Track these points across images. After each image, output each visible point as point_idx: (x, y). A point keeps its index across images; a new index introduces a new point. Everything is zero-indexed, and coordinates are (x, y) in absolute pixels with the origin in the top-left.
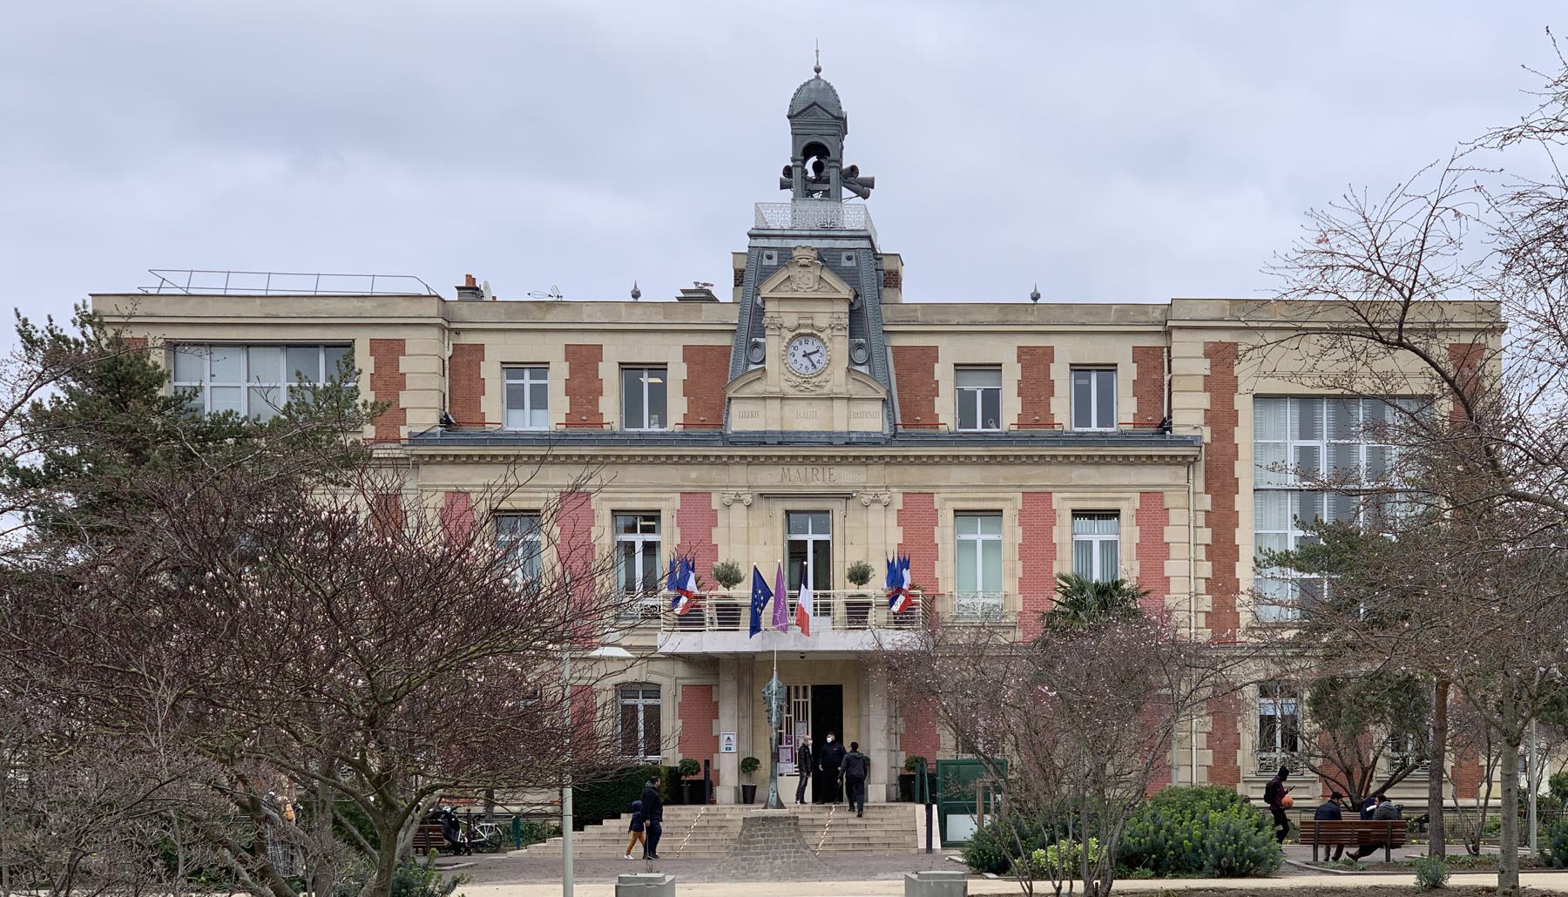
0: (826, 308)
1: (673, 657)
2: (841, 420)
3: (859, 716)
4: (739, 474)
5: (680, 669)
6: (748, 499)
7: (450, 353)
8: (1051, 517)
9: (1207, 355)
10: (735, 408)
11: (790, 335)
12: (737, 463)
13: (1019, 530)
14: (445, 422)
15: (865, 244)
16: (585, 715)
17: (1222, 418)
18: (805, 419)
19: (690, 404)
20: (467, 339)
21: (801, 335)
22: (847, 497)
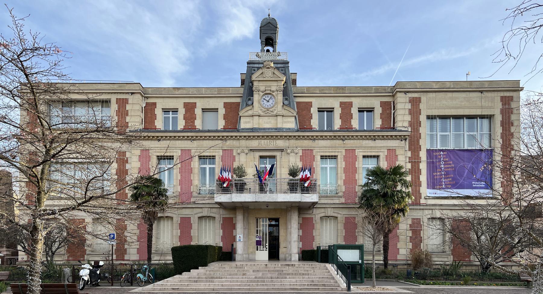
0: (275, 84)
1: (221, 205)
3: (286, 229)
4: (243, 143)
5: (222, 211)
6: (246, 151)
7: (145, 105)
8: (355, 158)
9: (410, 102)
10: (243, 120)
11: (262, 94)
12: (243, 139)
16: (310, 214)
17: (415, 124)
18: (267, 123)
20: (151, 101)
22: (282, 150)
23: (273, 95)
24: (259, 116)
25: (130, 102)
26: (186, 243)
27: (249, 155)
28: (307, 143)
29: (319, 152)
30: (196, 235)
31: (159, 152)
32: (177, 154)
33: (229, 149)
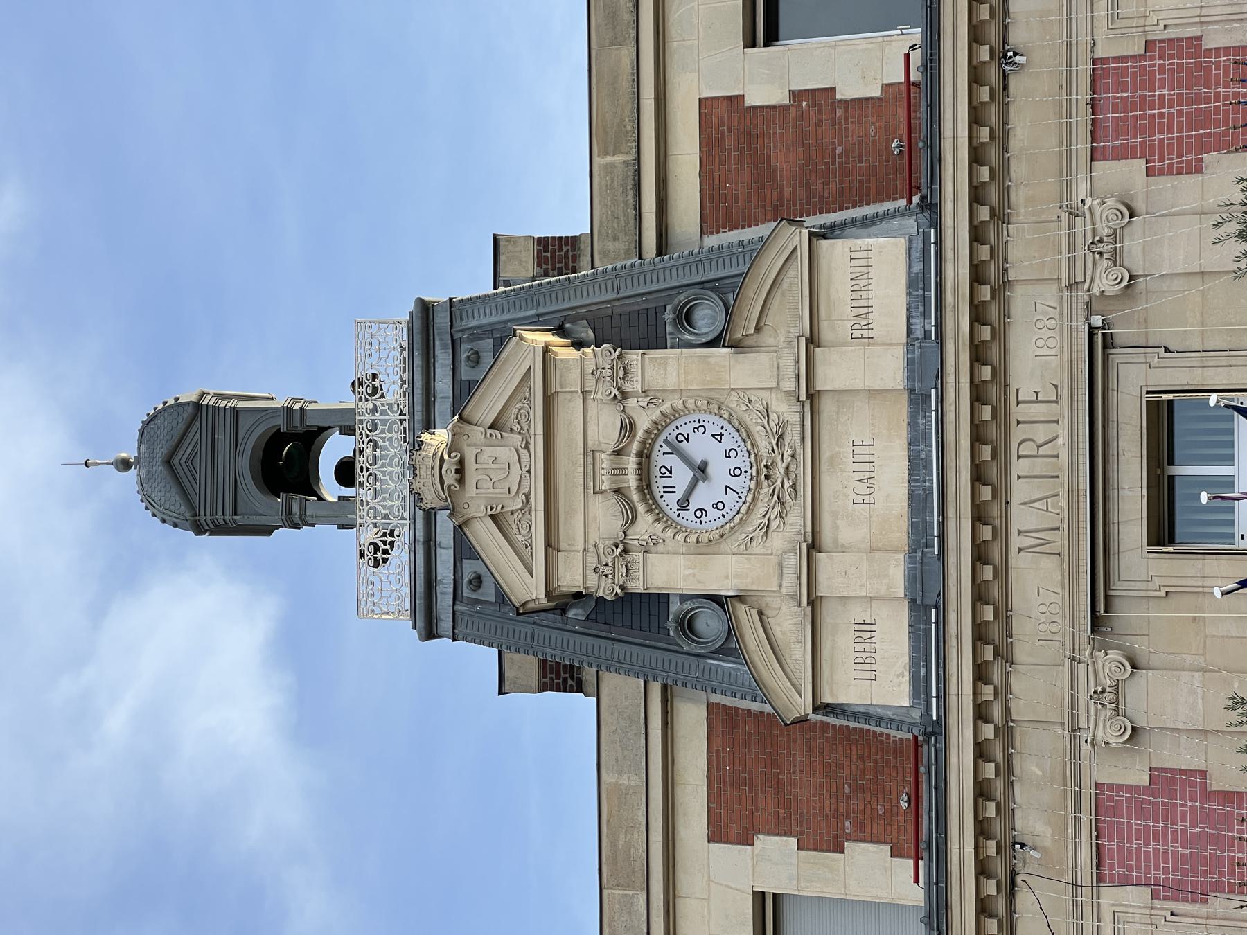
0: (570, 413)
4: (1035, 689)
6: (1110, 664)
10: (846, 689)
12: (1004, 691)
18: (870, 481)
21: (645, 486)
22: (1101, 344)
23: (657, 428)
24: (814, 546)
27: (1140, 646)
33: (1087, 818)
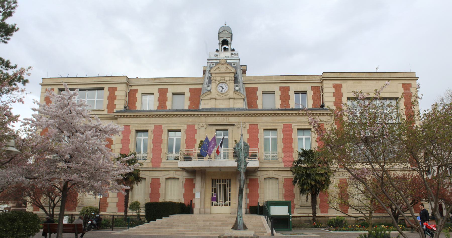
0: (228, 75)
1: (184, 169)
2: (232, 104)
4: (203, 119)
5: (185, 174)
6: (205, 126)
8: (291, 131)
11: (218, 82)
13: (282, 135)
14: (125, 108)
15: (238, 61)
18: (222, 104)
19: (190, 103)
22: (233, 125)
23: (227, 84)
24: (216, 99)
25: (118, 89)
26: (154, 201)
27: (207, 128)
28: (252, 120)
29: (263, 126)
30: (164, 192)
31: (137, 127)
32: (151, 128)
